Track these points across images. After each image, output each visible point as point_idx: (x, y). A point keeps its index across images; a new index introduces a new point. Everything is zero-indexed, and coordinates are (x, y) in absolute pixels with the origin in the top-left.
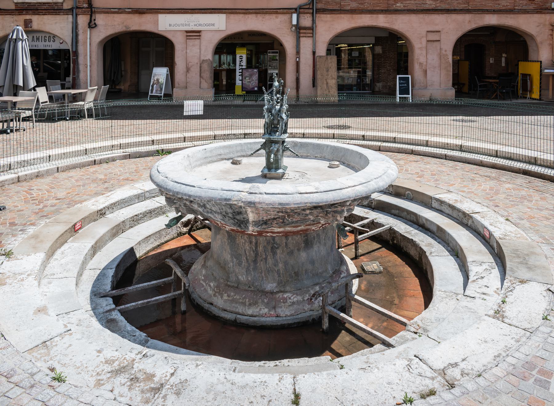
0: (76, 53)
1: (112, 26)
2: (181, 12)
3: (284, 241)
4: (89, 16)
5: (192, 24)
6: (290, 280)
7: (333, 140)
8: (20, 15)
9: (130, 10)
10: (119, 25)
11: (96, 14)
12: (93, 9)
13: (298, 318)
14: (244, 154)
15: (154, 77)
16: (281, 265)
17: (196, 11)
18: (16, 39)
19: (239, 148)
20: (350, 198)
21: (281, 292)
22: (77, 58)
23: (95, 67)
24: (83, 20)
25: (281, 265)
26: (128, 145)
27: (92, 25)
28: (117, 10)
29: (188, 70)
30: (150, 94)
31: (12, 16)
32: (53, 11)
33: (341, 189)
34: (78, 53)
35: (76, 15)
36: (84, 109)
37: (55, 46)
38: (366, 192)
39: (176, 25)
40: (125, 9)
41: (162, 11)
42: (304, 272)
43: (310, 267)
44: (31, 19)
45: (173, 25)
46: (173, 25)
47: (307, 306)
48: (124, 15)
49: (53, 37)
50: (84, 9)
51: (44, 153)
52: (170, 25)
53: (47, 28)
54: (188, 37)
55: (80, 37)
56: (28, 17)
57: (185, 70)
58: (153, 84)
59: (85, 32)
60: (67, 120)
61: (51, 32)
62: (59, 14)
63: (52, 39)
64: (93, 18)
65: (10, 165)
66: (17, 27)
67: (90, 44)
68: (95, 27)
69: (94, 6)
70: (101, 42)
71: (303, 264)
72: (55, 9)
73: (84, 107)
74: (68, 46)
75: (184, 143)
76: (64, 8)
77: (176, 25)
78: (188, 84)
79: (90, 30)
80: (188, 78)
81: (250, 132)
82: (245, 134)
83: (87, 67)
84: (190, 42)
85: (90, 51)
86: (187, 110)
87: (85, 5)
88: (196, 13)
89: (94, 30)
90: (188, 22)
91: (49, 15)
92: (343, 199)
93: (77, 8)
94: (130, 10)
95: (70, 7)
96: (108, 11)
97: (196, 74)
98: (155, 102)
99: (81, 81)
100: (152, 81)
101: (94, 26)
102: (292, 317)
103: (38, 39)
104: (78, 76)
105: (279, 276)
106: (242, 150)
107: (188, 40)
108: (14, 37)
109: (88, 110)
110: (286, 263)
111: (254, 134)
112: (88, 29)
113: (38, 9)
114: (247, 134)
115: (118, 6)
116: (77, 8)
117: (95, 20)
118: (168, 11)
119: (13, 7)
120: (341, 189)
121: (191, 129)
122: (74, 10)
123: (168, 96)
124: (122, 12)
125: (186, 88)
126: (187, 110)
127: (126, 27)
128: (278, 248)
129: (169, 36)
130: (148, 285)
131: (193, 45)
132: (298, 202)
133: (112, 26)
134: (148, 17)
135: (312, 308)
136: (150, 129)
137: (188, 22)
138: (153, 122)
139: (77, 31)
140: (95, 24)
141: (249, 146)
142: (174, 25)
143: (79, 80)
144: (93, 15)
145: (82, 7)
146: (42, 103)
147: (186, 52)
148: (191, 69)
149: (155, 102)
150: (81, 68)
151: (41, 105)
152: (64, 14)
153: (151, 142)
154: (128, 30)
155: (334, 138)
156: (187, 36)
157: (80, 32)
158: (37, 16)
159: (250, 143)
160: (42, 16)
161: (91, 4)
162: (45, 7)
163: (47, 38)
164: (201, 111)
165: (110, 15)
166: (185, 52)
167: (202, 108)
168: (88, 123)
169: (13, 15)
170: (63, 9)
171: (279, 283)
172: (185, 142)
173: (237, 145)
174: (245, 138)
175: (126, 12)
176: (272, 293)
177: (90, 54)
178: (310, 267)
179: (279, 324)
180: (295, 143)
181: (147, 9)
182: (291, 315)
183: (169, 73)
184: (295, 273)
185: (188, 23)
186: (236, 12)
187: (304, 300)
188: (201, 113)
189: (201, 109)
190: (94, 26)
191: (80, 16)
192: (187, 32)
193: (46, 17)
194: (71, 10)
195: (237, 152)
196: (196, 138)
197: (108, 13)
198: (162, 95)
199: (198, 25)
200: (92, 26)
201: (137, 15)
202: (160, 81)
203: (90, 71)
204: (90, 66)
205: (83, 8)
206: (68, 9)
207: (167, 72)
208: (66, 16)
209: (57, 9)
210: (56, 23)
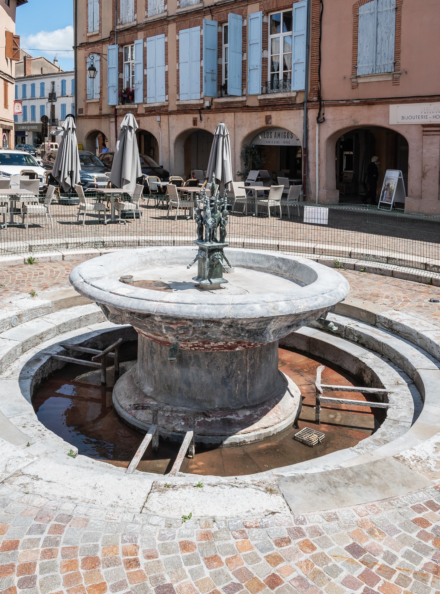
0: (306, 150)
1: (340, 120)
2: (425, 100)
3: (159, 349)
4: (318, 110)
5: (430, 115)
6: (163, 391)
7: (353, 271)
8: (262, 111)
9: (358, 101)
10: (347, 119)
11: (325, 108)
12: (323, 102)
13: (146, 427)
14: (244, 265)
15: (386, 181)
16: (156, 372)
17: (436, 98)
18: (219, 135)
19: (239, 257)
20: (150, 311)
21: (152, 398)
22: (307, 156)
23: (323, 166)
24: (313, 114)
25: (156, 372)
26: (251, 246)
27: (320, 120)
28: (345, 102)
29: (424, 175)
30: (380, 201)
31: (256, 113)
32: (287, 106)
33: (149, 300)
34: (308, 150)
35: (307, 109)
36: (267, 207)
37: (281, 142)
38: (174, 312)
39: (410, 118)
40: (354, 100)
41: (393, 100)
42: (177, 389)
43: (185, 388)
44: (270, 116)
45: (406, 118)
46: (406, 118)
47: (164, 422)
48: (352, 107)
49: (289, 134)
50: (313, 103)
51: (170, 238)
52: (403, 118)
53: (282, 124)
54: (425, 133)
55: (310, 133)
56: (268, 113)
57: (420, 175)
58: (384, 189)
59: (314, 128)
60: (253, 216)
61: (286, 128)
62: (292, 109)
63: (290, 136)
64: (322, 112)
65: (139, 241)
66: (221, 124)
67: (319, 141)
68: (323, 122)
69: (323, 99)
70: (330, 138)
71: (176, 380)
72: (289, 104)
73: (268, 205)
74: (300, 143)
75: (313, 255)
76: (297, 103)
77: (410, 118)
78: (423, 192)
79: (319, 126)
80: (424, 185)
81: (395, 257)
82: (388, 258)
83: (316, 166)
84: (428, 140)
85: (319, 149)
86: (308, 217)
87: (315, 99)
88: (435, 101)
89: (323, 126)
90: (425, 113)
91: (285, 111)
92: (140, 310)
93: (308, 101)
94: (358, 101)
95: (302, 102)
96: (336, 104)
97: (434, 181)
98: (384, 212)
99: (311, 180)
100: (384, 185)
101: (323, 120)
102: (142, 423)
103: (279, 135)
104: (308, 175)
105: (156, 383)
106: (242, 260)
107: (424, 137)
108: (217, 133)
109: (272, 208)
110: (161, 373)
111: (399, 260)
112: (317, 125)
113: (276, 105)
114: (390, 258)
115: (346, 98)
116: (308, 101)
117: (324, 114)
118: (401, 100)
119: (257, 104)
120: (149, 300)
121: (327, 240)
122: (305, 104)
123: (399, 206)
124: (350, 104)
125: (421, 198)
126: (308, 217)
127: (354, 121)
128: (154, 353)
129: (402, 131)
130: (94, 352)
131: (431, 144)
132: (101, 299)
133: (340, 120)
134: (378, 108)
135: (165, 426)
136: (302, 235)
137: (425, 113)
138: (313, 228)
139: (308, 126)
140: (324, 118)
141: (252, 256)
142: (408, 118)
143: (309, 179)
144: (322, 109)
145: (312, 100)
146: (237, 197)
147: (422, 152)
148: (428, 174)
149: (384, 212)
150: (311, 166)
151: (236, 199)
152: (297, 109)
153: (352, 256)
154: (357, 124)
155: (354, 269)
156: (423, 131)
157: (310, 128)
158: (275, 112)
159: (254, 254)
160: (279, 112)
161: (320, 96)
162: (281, 102)
163: (286, 135)
164: (325, 221)
165: (338, 108)
166: (420, 151)
167: (326, 216)
168: (272, 221)
169: (257, 112)
170: (296, 104)
171: (155, 389)
172: (314, 253)
173: (238, 253)
174: (387, 263)
175: (354, 103)
176: (146, 396)
177: (319, 152)
178: (185, 388)
179: (132, 423)
180: (296, 263)
181: (377, 99)
182: (143, 421)
183: (402, 177)
184: (168, 386)
185: (425, 115)
186: (408, 101)
187: (164, 415)
188: (326, 222)
189: (325, 218)
190: (323, 120)
191: (311, 110)
192: (424, 126)
193: (282, 112)
194: (303, 104)
195: (237, 260)
196: (327, 251)
197: (335, 105)
198: (392, 203)
199: (438, 117)
200: (321, 121)
201: (366, 107)
202: (391, 186)
203: (319, 170)
204: (319, 165)
205: (313, 101)
206: (300, 104)
207: (400, 175)
208: (299, 111)
209: (291, 104)
210: (290, 119)
